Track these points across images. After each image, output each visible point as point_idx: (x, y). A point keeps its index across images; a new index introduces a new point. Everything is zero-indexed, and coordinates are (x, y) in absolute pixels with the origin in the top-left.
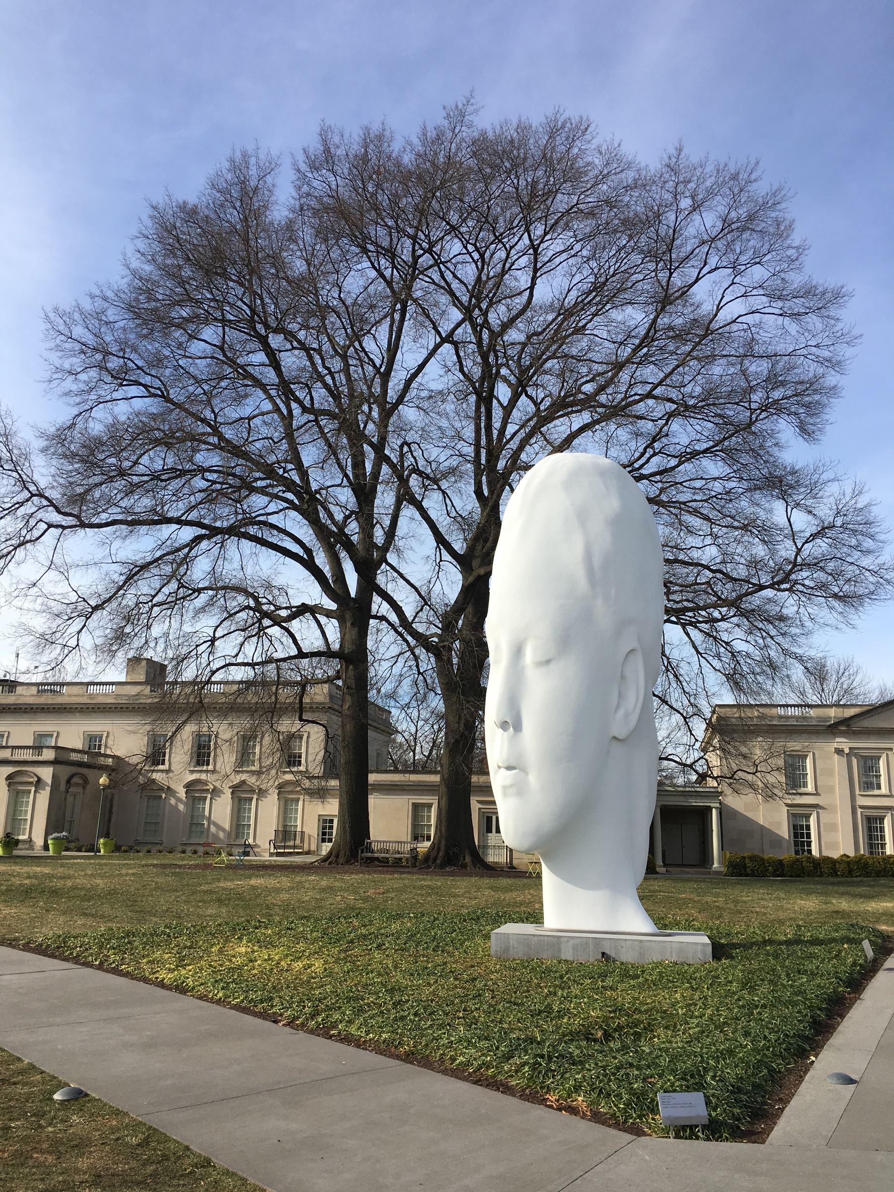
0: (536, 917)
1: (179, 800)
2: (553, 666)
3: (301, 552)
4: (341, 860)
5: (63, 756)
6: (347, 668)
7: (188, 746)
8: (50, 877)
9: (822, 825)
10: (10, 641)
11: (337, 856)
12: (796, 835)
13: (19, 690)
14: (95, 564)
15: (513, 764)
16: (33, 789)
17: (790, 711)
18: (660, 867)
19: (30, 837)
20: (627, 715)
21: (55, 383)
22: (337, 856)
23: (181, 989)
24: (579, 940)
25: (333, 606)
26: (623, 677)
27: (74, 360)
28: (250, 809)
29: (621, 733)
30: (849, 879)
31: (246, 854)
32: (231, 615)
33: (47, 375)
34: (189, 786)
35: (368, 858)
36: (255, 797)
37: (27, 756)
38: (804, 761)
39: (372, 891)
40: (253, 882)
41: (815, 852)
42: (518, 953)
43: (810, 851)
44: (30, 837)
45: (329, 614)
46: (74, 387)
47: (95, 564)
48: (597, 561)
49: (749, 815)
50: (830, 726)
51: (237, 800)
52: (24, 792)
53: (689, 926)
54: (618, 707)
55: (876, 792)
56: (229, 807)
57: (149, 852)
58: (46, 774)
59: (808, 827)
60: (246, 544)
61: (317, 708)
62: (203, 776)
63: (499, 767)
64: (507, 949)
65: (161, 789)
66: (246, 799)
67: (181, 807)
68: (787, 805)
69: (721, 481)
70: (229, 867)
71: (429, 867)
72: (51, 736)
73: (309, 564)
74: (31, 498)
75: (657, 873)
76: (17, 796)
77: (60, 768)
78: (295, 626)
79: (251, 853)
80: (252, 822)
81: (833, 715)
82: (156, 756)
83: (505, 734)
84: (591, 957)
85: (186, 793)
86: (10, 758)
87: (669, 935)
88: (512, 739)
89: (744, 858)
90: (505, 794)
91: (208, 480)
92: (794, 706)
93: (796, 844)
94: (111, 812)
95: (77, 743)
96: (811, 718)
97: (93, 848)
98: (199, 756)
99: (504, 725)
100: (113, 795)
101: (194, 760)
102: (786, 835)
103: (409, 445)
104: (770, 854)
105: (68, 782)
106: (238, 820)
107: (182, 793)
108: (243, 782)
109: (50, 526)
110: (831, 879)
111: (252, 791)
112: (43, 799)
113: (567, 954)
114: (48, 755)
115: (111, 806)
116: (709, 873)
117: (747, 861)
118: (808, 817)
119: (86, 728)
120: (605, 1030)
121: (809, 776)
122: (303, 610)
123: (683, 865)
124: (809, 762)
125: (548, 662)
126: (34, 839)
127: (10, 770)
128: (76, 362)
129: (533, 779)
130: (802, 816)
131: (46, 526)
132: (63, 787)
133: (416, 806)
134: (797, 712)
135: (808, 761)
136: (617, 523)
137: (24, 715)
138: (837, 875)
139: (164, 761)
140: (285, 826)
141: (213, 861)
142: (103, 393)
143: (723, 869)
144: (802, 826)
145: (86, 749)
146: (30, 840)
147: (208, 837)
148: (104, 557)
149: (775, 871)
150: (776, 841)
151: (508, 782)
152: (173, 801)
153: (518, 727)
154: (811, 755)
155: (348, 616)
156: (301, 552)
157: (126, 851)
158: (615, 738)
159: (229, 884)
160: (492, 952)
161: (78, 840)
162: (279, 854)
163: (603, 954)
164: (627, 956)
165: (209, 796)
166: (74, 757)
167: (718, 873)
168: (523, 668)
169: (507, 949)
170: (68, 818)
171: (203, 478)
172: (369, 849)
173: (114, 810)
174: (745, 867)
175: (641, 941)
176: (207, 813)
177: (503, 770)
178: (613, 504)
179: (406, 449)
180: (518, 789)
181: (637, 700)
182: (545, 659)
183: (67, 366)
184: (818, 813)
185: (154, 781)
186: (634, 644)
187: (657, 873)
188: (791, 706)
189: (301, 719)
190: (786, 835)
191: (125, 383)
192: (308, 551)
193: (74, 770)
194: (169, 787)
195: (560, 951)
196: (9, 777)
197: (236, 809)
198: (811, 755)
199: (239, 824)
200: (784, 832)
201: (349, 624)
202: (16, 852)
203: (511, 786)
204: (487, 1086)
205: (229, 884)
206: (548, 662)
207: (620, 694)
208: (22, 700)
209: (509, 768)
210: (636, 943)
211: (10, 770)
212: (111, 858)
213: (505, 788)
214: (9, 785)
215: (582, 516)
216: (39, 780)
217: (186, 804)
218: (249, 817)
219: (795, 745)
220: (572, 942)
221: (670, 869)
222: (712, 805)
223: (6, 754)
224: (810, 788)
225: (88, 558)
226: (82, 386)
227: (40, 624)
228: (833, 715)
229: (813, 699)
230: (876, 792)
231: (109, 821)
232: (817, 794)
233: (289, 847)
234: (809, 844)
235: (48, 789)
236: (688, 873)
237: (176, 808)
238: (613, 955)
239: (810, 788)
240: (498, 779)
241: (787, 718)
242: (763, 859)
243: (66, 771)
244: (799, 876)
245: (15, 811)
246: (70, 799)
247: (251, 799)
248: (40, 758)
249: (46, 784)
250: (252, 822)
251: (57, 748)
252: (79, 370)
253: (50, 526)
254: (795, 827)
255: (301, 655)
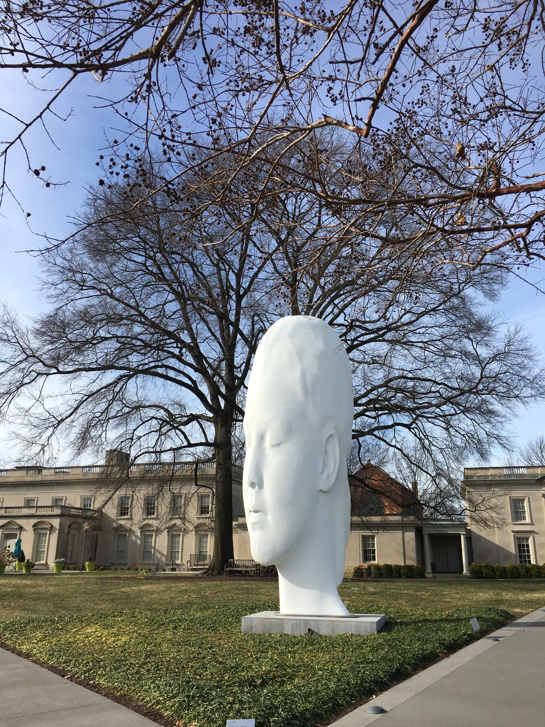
0: (276, 607)
1: (137, 537)
2: (282, 447)
3: (190, 383)
4: (215, 573)
5: (66, 512)
6: (219, 452)
7: (142, 502)
8: (25, 586)
9: (536, 544)
10: (5, 443)
11: (213, 570)
12: (520, 551)
13: (44, 472)
14: (62, 395)
15: (258, 509)
16: (48, 532)
17: (522, 471)
18: (430, 573)
19: (46, 562)
20: (328, 476)
21: (44, 291)
22: (213, 570)
23: (27, 656)
24: (295, 621)
25: (210, 415)
26: (326, 452)
27: (55, 277)
28: (179, 541)
29: (325, 487)
30: (380, 579)
31: (173, 570)
32: (144, 423)
33: (39, 286)
34: (142, 528)
35: (231, 571)
36: (182, 534)
37: (48, 512)
38: (523, 503)
39: (209, 592)
40: (143, 588)
41: (533, 562)
42: (258, 630)
43: (530, 561)
44: (46, 562)
45: (208, 419)
46: (54, 293)
47: (62, 395)
48: (309, 381)
49: (489, 538)
50: (538, 480)
51: (171, 536)
52: (43, 534)
53: (369, 611)
54: (323, 471)
55: (523, 522)
56: (166, 541)
57: (116, 569)
58: (56, 522)
59: (528, 546)
60: (160, 381)
61: (209, 478)
62: (150, 522)
63: (250, 511)
64: (251, 628)
65: (126, 530)
66: (176, 535)
67: (139, 542)
68: (513, 532)
69: (437, 328)
70: (147, 578)
71: (267, 576)
72: (62, 499)
73: (195, 389)
74: (27, 358)
75: (426, 577)
76: (172, 538)
77: (64, 519)
78: (186, 429)
79: (177, 569)
80: (180, 550)
81: (540, 473)
82: (123, 510)
83: (254, 490)
84: (302, 632)
85: (141, 532)
86: (35, 514)
87: (357, 617)
88: (257, 494)
89: (481, 566)
90: (254, 529)
91: (119, 343)
92: (524, 467)
93: (521, 557)
94: (96, 545)
95: (78, 504)
96: (526, 475)
97: (84, 568)
98: (148, 509)
99: (252, 485)
100: (97, 535)
101: (200, 511)
102: (513, 551)
103: (258, 315)
104: (507, 565)
105: (69, 527)
106: (172, 549)
107: (138, 533)
108: (175, 524)
109: (39, 374)
110: (537, 579)
111: (180, 530)
112: (54, 539)
113: (288, 630)
114: (57, 511)
115: (97, 542)
116: (461, 577)
117: (483, 569)
118: (527, 539)
119: (82, 494)
120: (264, 679)
121: (526, 513)
122: (193, 418)
123: (448, 572)
124: (526, 503)
125: (279, 444)
126: (49, 563)
127: (35, 521)
128: (56, 278)
129: (270, 518)
130: (523, 539)
131: (36, 375)
132: (66, 531)
133: (365, 538)
134: (505, 472)
135: (525, 502)
136: (321, 357)
137: (47, 487)
138: (541, 577)
139: (154, 512)
140: (200, 552)
141: (161, 573)
142: (70, 295)
143: (469, 574)
144: (523, 545)
145: (82, 507)
146: (46, 564)
147: (154, 560)
148: (67, 391)
149: (501, 575)
150: (508, 554)
151: (255, 520)
152: (134, 538)
153: (261, 486)
154: (527, 499)
155: (219, 420)
156: (190, 383)
157: (102, 570)
158: (321, 490)
159: (128, 589)
160: (243, 630)
161: (76, 563)
162: (193, 570)
163: (309, 630)
164: (324, 631)
165: (154, 534)
166: (73, 512)
167: (466, 577)
168: (264, 449)
169: (251, 628)
170: (70, 549)
171: (117, 341)
172: (233, 565)
173: (99, 544)
174: (482, 572)
175: (333, 621)
176: (153, 545)
177: (252, 513)
178: (320, 345)
179: (256, 318)
180: (261, 525)
181: (335, 466)
182: (278, 442)
183: (51, 280)
184: (533, 537)
185: (121, 525)
186: (333, 431)
187: (426, 577)
188: (522, 467)
189: (196, 485)
190: (514, 552)
191: (84, 288)
192: (194, 382)
193: (74, 520)
194: (130, 529)
195: (283, 629)
196: (35, 525)
197: (198, 543)
198: (527, 499)
199: (172, 552)
200: (512, 549)
201: (219, 425)
202: (32, 571)
203: (257, 523)
204: (145, 715)
205: (128, 589)
206: (279, 444)
207: (324, 464)
208: (46, 478)
209: (256, 512)
210: (330, 623)
211: (35, 521)
212: (93, 574)
213: (253, 524)
214: (35, 530)
215: (300, 354)
216: (52, 526)
217: (141, 539)
218: (178, 547)
219: (517, 493)
220: (290, 623)
221: (435, 575)
222: (461, 533)
223: (2, 512)
224: (528, 521)
225: (57, 392)
226: (58, 292)
227: (25, 432)
228: (540, 473)
229: (537, 463)
230: (523, 522)
231: (96, 551)
232: (532, 524)
233: (201, 565)
234: (529, 557)
235: (57, 532)
236: (447, 577)
237: (135, 542)
238: (316, 631)
239: (528, 521)
240: (250, 519)
241: (522, 475)
242: (493, 568)
243: (67, 521)
244: (516, 578)
245: (38, 546)
246: (70, 538)
247: (179, 535)
248: (53, 513)
249: (56, 529)
250: (180, 550)
251: (62, 507)
252: (58, 282)
253: (39, 374)
254: (519, 546)
255: (190, 445)
